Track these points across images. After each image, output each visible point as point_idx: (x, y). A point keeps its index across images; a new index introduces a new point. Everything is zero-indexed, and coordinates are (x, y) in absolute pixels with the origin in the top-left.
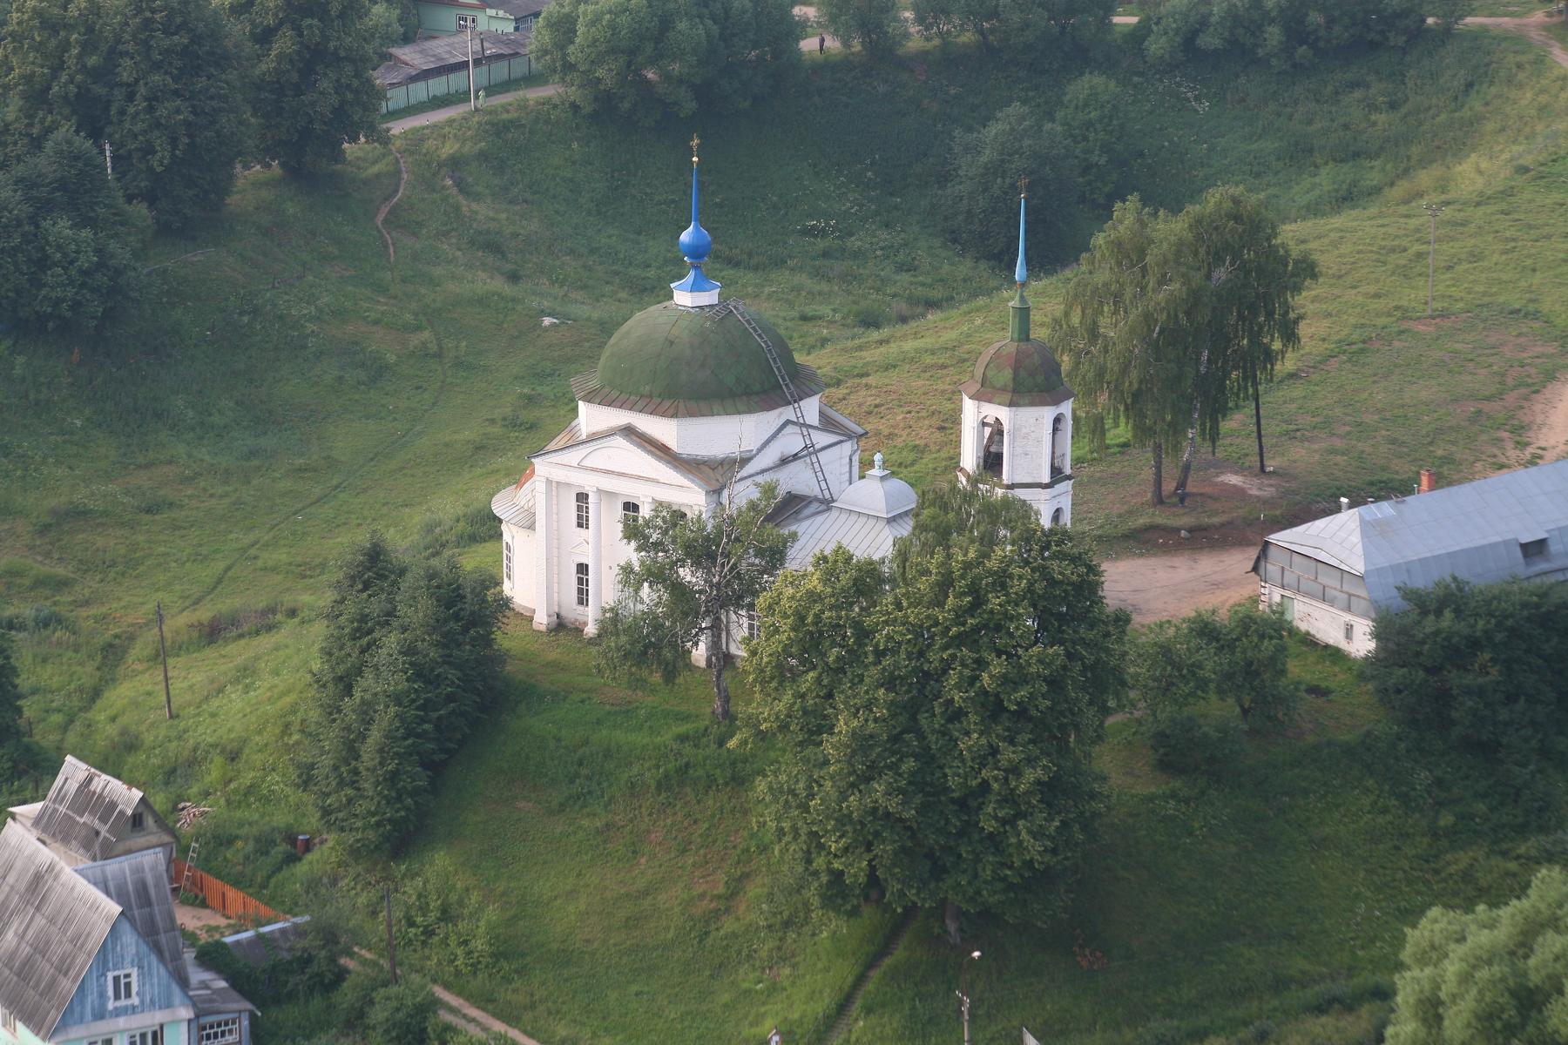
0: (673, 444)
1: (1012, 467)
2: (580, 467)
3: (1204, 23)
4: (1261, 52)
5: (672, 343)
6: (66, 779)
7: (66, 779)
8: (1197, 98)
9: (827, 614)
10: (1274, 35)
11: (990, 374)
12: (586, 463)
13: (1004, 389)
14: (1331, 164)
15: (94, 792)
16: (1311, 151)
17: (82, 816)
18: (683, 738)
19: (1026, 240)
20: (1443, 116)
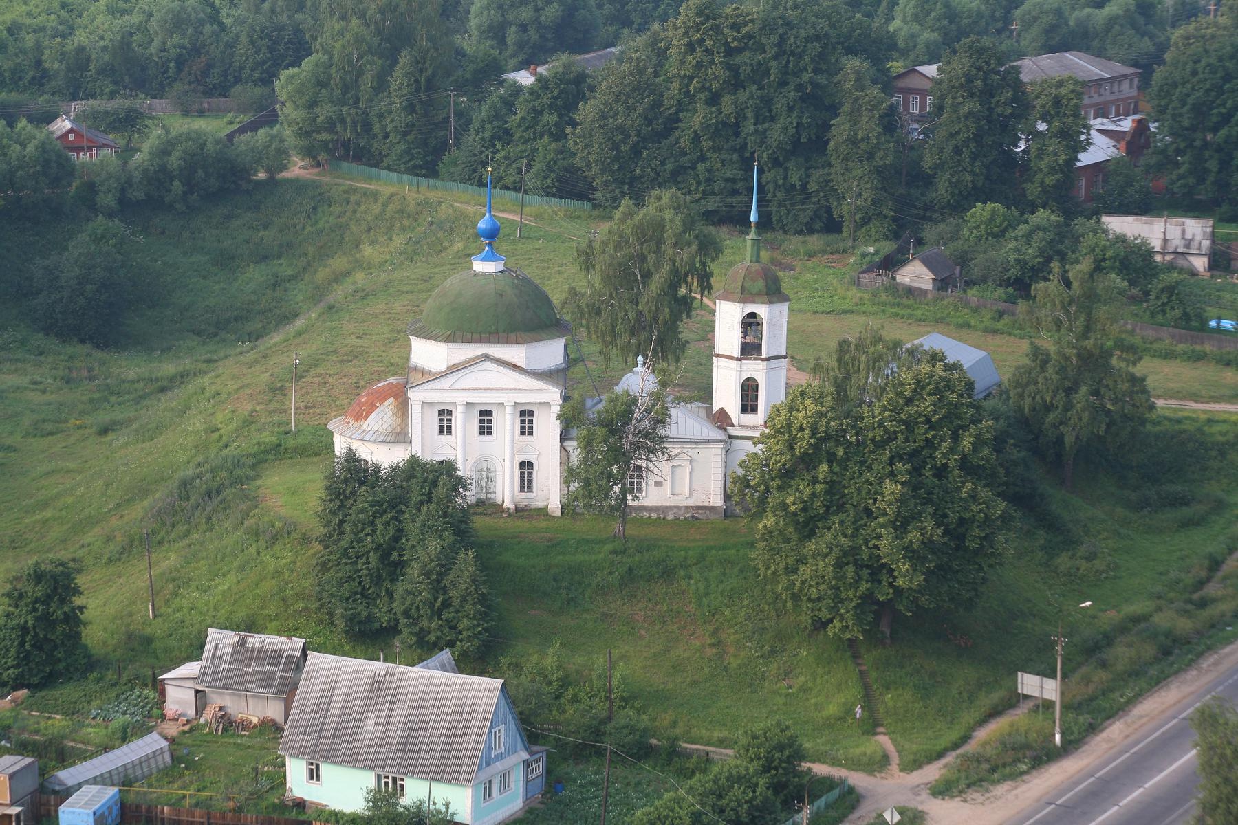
0: (522, 364)
1: (768, 347)
2: (453, 389)
3: (129, 182)
4: (167, 200)
5: (501, 295)
6: (217, 645)
7: (217, 645)
8: (132, 234)
9: (833, 423)
10: (177, 187)
11: (746, 285)
12: (454, 386)
13: (759, 294)
14: (252, 266)
15: (253, 648)
16: (233, 258)
17: (250, 667)
18: (614, 552)
19: (758, 194)
20: (308, 229)
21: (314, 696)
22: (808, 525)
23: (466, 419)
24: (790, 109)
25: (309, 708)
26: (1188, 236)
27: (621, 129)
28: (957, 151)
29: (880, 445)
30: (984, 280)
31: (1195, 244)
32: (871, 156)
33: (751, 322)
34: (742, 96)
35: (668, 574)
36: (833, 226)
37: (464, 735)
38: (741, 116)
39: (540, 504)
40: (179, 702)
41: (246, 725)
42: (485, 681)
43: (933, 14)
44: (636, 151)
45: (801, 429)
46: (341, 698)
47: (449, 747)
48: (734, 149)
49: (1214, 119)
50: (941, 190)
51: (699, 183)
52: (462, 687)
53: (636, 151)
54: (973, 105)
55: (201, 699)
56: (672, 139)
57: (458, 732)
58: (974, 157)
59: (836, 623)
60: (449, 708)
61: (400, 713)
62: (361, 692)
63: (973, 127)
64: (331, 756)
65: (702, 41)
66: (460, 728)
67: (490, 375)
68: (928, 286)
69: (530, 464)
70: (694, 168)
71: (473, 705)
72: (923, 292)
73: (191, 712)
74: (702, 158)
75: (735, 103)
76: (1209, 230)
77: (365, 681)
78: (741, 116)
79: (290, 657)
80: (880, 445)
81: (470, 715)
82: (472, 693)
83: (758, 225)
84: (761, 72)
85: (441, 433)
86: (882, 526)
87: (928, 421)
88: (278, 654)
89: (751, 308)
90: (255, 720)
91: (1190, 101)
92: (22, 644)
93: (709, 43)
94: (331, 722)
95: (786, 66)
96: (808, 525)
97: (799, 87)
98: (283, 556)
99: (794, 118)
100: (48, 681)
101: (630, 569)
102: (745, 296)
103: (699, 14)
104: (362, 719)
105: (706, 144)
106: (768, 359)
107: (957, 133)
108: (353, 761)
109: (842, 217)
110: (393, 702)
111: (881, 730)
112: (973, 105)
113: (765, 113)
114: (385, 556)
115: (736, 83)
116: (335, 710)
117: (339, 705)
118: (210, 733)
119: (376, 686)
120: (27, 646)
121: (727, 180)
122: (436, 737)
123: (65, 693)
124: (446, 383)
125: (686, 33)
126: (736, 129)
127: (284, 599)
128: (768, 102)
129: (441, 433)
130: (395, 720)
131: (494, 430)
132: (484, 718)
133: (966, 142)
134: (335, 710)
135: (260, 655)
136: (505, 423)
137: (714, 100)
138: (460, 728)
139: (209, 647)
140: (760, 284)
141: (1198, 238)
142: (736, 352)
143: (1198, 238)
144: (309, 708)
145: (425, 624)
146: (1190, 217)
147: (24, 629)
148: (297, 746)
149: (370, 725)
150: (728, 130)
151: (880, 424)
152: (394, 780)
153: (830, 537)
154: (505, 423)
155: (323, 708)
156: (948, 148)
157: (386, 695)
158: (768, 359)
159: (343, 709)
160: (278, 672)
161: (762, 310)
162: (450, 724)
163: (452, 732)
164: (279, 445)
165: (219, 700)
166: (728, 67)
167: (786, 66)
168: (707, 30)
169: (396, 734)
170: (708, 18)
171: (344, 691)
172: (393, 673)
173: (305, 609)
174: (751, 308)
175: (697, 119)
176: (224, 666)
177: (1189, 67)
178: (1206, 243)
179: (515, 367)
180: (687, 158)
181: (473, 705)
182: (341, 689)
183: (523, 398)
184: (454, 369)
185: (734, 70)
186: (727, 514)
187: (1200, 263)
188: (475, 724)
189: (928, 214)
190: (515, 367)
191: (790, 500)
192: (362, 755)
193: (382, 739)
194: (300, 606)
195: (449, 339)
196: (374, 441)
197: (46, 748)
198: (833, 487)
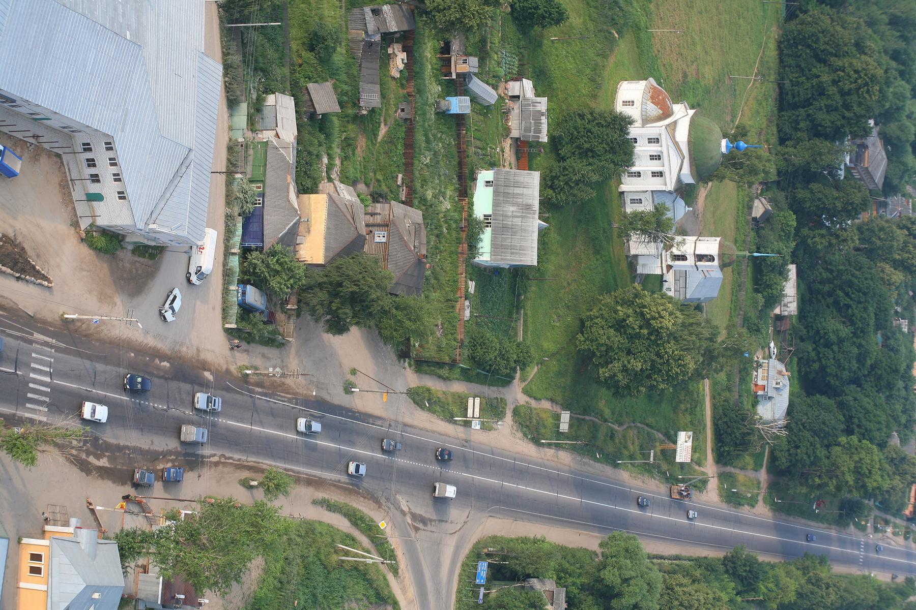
2: (668, 146)
13: (723, 261)
21: (521, 179)
22: (620, 326)
23: (657, 151)
24: (832, 122)
25: (516, 178)
26: (789, 305)
27: (818, 40)
28: (820, 199)
29: (658, 354)
30: (759, 237)
31: (785, 308)
32: (815, 161)
33: (711, 258)
34: (837, 97)
35: (597, 252)
36: (782, 141)
37: (512, 253)
38: (829, 97)
39: (623, 181)
40: (513, 88)
41: (507, 120)
42: (535, 258)
43: (898, 102)
44: (809, 46)
45: (661, 323)
46: (522, 192)
47: (506, 247)
48: (813, 94)
49: (846, 289)
50: (801, 194)
51: (797, 78)
52: (532, 247)
53: (809, 46)
54: (839, 205)
55: (516, 98)
56: (815, 63)
57: (513, 251)
58: (818, 206)
59: (583, 339)
60: (523, 244)
61: (518, 221)
62: (525, 201)
63: (831, 206)
64: (496, 193)
65: (861, 77)
66: (515, 251)
67: (675, 162)
68: (753, 215)
69: (640, 176)
70: (804, 75)
71: (525, 254)
72: (750, 214)
73: (510, 94)
74: (808, 79)
75: (834, 94)
76: (792, 313)
77: (530, 202)
78: (829, 97)
79: (539, 137)
80: (658, 354)
81: (520, 254)
82: (530, 252)
83: (753, 256)
84: (847, 106)
85: (649, 139)
86: (623, 362)
87: (670, 371)
88: (540, 131)
89: (716, 258)
90: (510, 124)
91: (853, 279)
92: (530, 8)
93: (859, 81)
94: (511, 190)
95: (852, 119)
96: (620, 326)
97: (843, 126)
98: (584, 88)
99: (829, 124)
100: (515, 19)
101: (597, 238)
102: (721, 255)
103: (873, 76)
104: (514, 204)
105: (814, 81)
106: (696, 265)
107: (827, 199)
108: (496, 204)
109: (786, 146)
110: (522, 217)
111: (539, 366)
112: (839, 205)
113: (830, 109)
114: (588, 150)
115: (843, 93)
116: (517, 191)
117: (519, 192)
118: (502, 106)
119: (528, 207)
120: (530, 11)
121: (798, 92)
122: (510, 240)
123: (512, 29)
124: (670, 143)
125: (864, 69)
126: (822, 94)
127: (566, 99)
128: (836, 109)
129: (649, 139)
130: (515, 220)
131: (652, 161)
132: (521, 261)
133: (823, 203)
134: (517, 191)
135: (538, 123)
136: (656, 166)
137: (835, 82)
138: (515, 251)
139: (539, 99)
140: (727, 261)
141: (788, 309)
142: (697, 252)
143: (788, 309)
144: (516, 178)
145: (562, 178)
146: (798, 304)
147: (537, 8)
148: (499, 177)
149: (512, 209)
150: (821, 91)
151: (666, 353)
152: (490, 223)
153: (616, 339)
154: (656, 166)
155: (517, 185)
156: (820, 195)
157: (525, 213)
158: (696, 265)
159: (517, 194)
160: (532, 134)
161: (716, 263)
162: (516, 246)
163: (512, 247)
164: (640, 30)
165: (516, 107)
166: (850, 90)
167: (852, 119)
168: (864, 79)
169: (509, 222)
170: (871, 79)
171: (525, 193)
172: (534, 214)
173: (563, 110)
174: (716, 258)
175: (826, 78)
176: (531, 108)
177: (869, 276)
178: (786, 313)
179: (681, 169)
180: (807, 72)
181: (525, 254)
182: (525, 191)
183: (667, 175)
184: (676, 144)
185: (849, 93)
186: (627, 257)
187: (777, 311)
188: (517, 257)
189: (791, 185)
190: (681, 169)
191: (631, 319)
192: (499, 208)
193: (507, 216)
194: (564, 107)
195: (689, 142)
196: (642, 111)
197: (484, 51)
198: (638, 336)
